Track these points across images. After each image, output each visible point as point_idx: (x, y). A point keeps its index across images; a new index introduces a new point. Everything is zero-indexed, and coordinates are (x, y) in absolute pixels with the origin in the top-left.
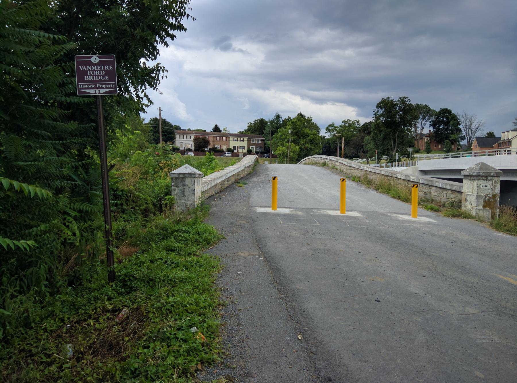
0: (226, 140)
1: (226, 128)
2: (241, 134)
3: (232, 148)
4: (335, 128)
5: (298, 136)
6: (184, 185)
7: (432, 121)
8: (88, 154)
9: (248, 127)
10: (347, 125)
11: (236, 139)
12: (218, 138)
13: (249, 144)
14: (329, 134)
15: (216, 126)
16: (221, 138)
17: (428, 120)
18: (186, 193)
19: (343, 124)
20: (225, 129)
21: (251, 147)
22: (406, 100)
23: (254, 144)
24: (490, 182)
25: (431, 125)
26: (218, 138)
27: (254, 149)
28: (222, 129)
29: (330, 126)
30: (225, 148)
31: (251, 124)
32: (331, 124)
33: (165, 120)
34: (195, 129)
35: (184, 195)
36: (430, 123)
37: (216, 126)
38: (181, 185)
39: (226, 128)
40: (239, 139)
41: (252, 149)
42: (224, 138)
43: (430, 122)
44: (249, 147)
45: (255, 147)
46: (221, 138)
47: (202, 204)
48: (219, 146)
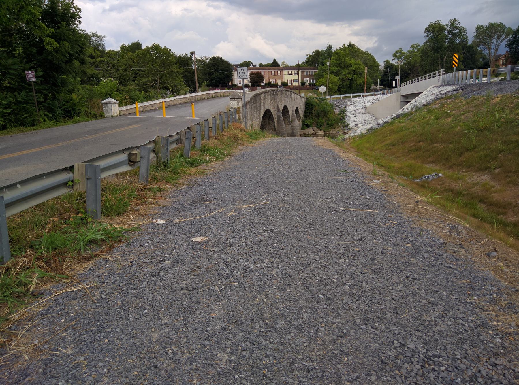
0: (281, 74)
1: (284, 62)
2: (298, 67)
3: (287, 82)
4: (403, 54)
5: (341, 67)
6: (107, 107)
7: (509, 40)
8: (499, 99)
9: (307, 59)
10: (416, 50)
11: (290, 72)
12: (273, 72)
13: (303, 77)
14: (396, 60)
15: (275, 60)
16: (276, 72)
17: (504, 39)
18: (109, 111)
19: (411, 49)
20: (283, 63)
21: (305, 79)
22: (456, 23)
23: (307, 77)
24: (236, 101)
25: (507, 45)
26: (273, 72)
27: (307, 82)
28: (280, 63)
29: (397, 52)
30: (280, 82)
31: (310, 56)
32: (399, 50)
33: (221, 58)
34: (266, 63)
35: (108, 112)
36: (506, 43)
37: (275, 60)
38: (106, 107)
39: (284, 62)
40: (293, 73)
41: (306, 82)
42: (279, 72)
43: (507, 42)
44: (302, 80)
45: (308, 79)
46: (276, 72)
47: (490, 224)
48: (274, 80)
